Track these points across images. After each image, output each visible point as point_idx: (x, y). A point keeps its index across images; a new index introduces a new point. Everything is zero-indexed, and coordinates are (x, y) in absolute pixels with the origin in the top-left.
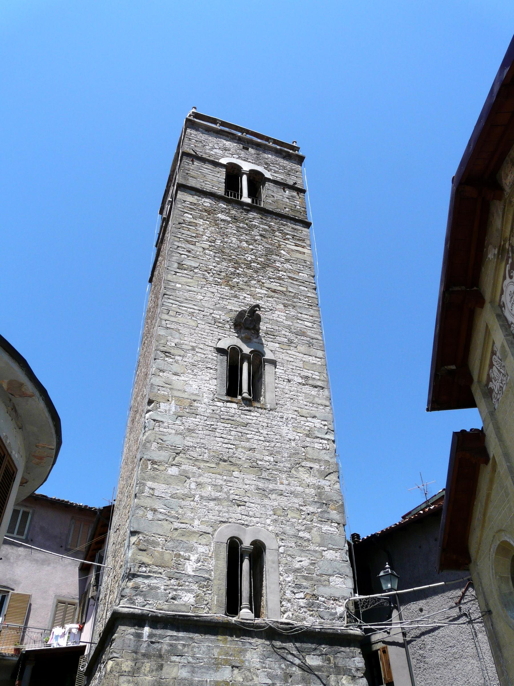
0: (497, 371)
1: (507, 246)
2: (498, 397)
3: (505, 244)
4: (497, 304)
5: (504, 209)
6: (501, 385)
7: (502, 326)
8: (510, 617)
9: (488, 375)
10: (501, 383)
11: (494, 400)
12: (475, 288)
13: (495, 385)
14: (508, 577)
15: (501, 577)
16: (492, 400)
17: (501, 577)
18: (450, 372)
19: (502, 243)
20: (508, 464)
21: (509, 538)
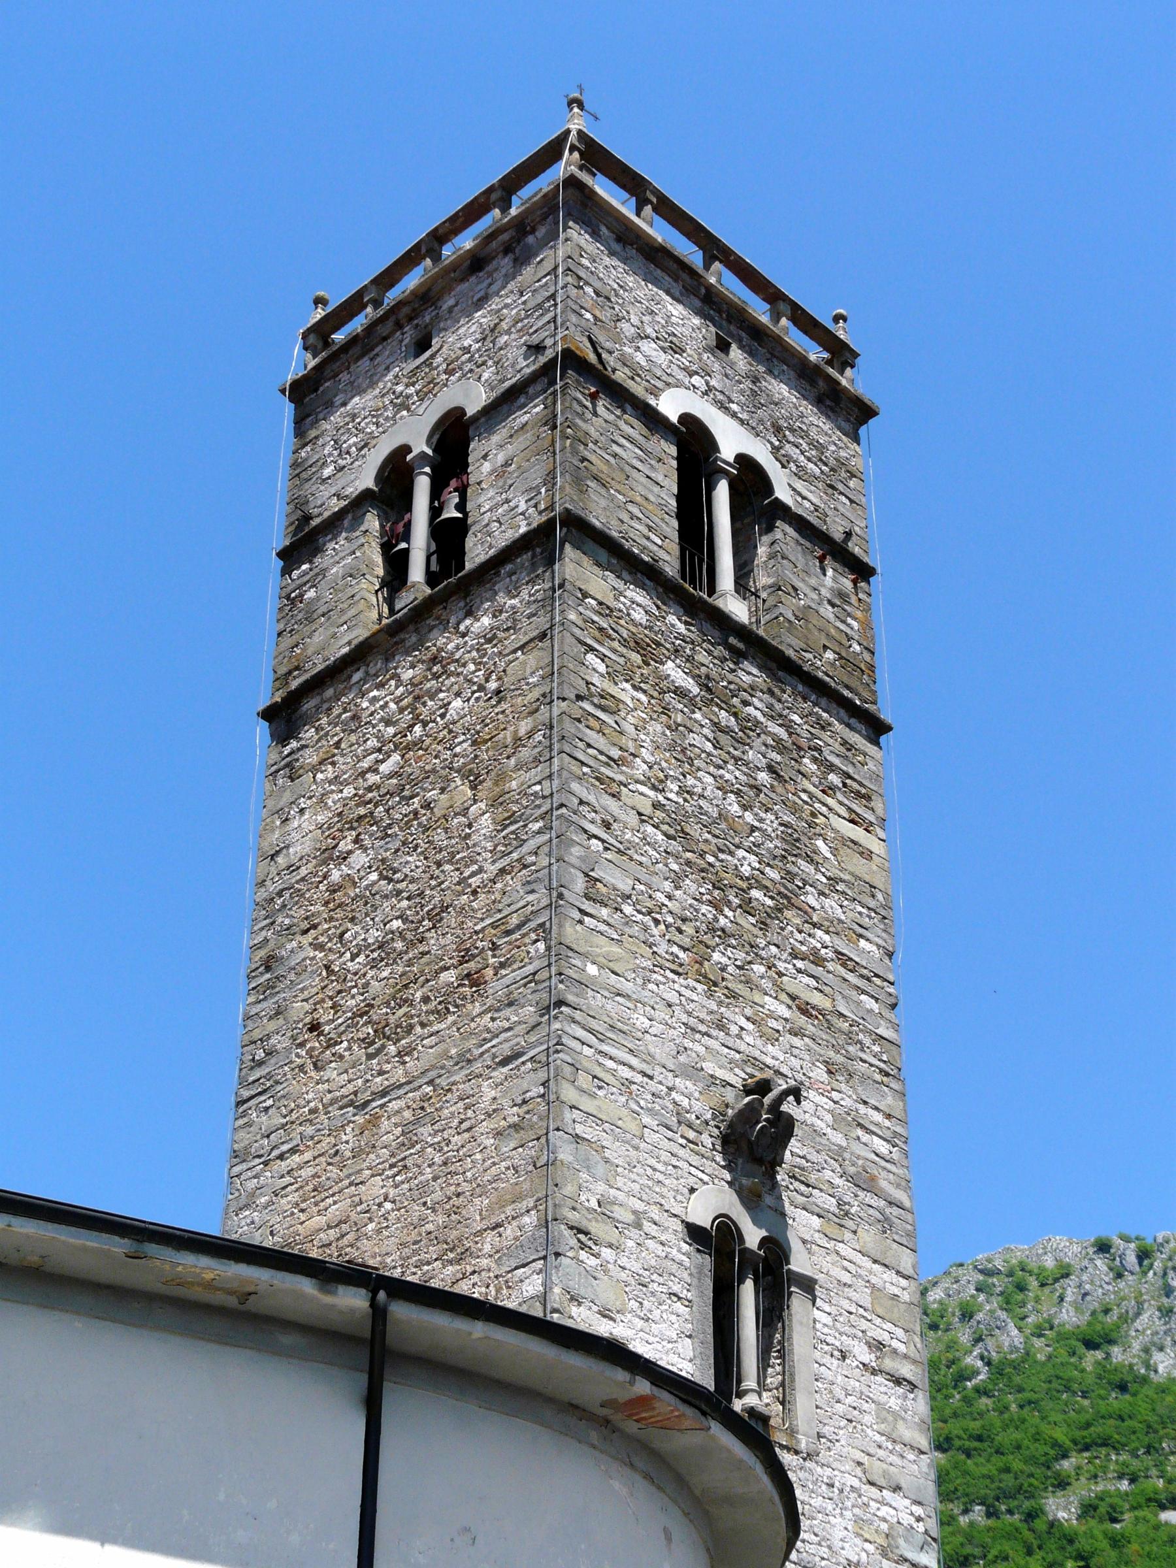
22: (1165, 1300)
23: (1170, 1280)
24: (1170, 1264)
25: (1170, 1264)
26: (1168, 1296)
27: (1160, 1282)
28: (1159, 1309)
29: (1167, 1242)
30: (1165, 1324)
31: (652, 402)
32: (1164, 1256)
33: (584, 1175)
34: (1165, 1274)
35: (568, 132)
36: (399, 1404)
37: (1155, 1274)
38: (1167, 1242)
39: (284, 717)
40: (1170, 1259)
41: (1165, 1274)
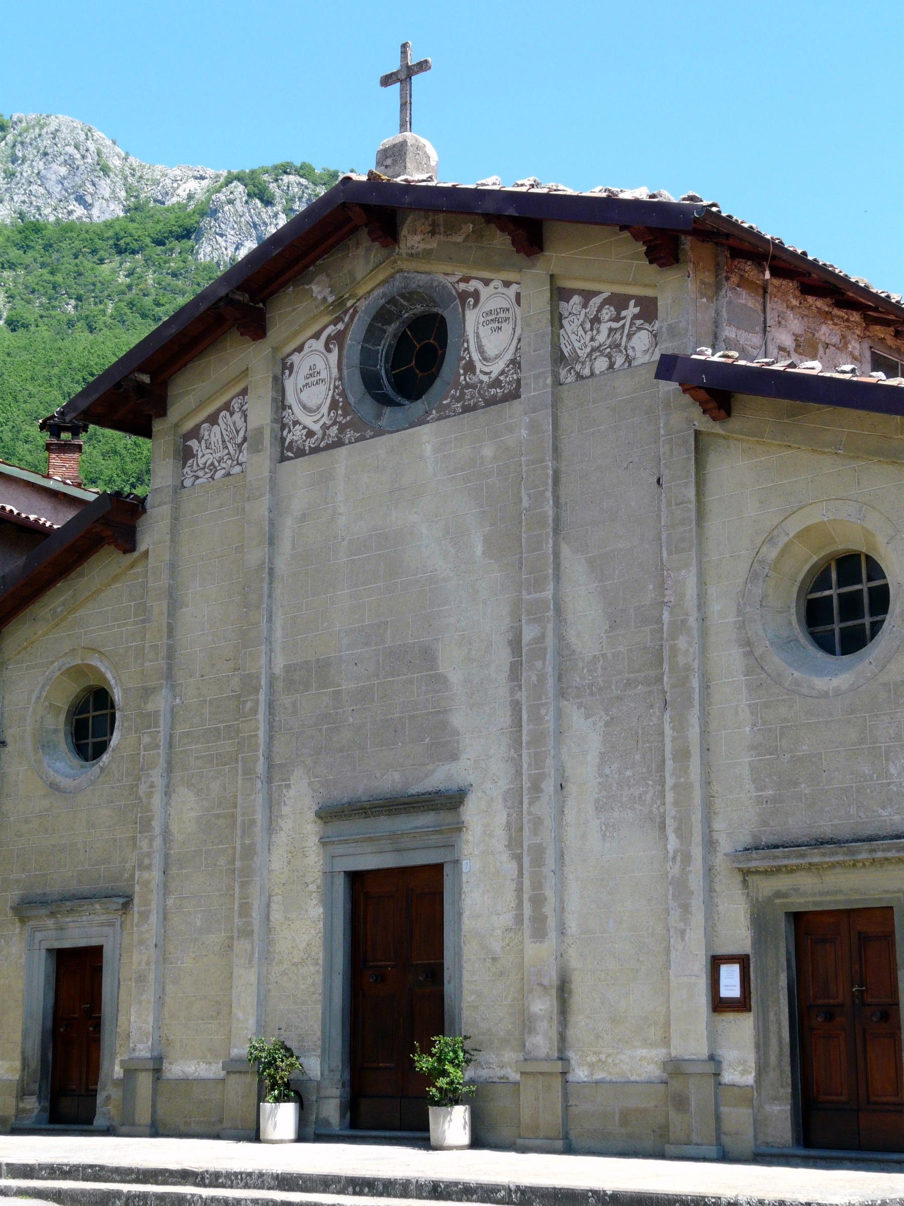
0: (219, 436)
1: (349, 304)
2: (200, 473)
3: (348, 299)
4: (281, 355)
5: (381, 264)
6: (216, 464)
7: (274, 400)
8: (46, 765)
9: (198, 427)
10: (219, 462)
11: (187, 469)
12: (261, 305)
13: (204, 456)
14: (60, 709)
15: (51, 705)
16: (184, 467)
17: (51, 705)
18: (140, 386)
19: (346, 296)
20: (171, 582)
21: (107, 668)
22: (10, 165)
23: (17, 151)
24: (19, 139)
25: (19, 139)
26: (13, 163)
27: (9, 151)
28: (5, 172)
29: (20, 122)
30: (7, 184)
31: (755, 1086)
32: (16, 132)
33: (769, 793)
34: (14, 146)
35: (701, 201)
36: (322, 1095)
37: (6, 144)
38: (20, 122)
39: (247, 369)
40: (20, 135)
41: (14, 146)
